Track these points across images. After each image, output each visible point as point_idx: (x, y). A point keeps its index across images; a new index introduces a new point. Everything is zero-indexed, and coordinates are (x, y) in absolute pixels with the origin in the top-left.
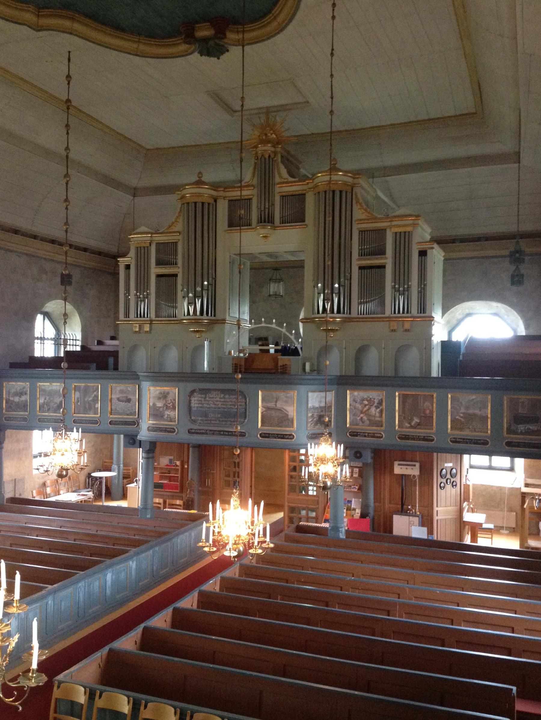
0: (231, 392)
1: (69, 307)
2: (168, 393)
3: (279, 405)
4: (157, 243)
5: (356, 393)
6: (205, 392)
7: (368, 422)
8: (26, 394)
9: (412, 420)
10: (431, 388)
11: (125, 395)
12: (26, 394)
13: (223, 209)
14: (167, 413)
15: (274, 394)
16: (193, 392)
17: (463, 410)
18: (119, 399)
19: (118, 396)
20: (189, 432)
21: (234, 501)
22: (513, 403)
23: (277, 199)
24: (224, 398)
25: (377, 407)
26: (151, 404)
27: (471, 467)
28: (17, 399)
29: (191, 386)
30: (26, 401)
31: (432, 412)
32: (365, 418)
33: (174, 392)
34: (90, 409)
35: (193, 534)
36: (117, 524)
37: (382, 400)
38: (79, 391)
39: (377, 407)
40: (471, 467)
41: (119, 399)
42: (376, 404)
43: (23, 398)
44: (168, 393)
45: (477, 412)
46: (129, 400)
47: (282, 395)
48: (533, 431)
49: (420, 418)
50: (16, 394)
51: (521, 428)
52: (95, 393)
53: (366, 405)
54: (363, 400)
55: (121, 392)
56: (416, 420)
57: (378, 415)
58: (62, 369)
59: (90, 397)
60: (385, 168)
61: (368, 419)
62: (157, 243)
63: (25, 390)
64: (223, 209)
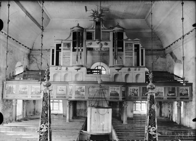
1: (195, 97)
2: (82, 87)
3: (115, 90)
5: (131, 87)
6: (93, 87)
7: (134, 95)
8: (27, 89)
9: (145, 94)
10: (137, 85)
11: (62, 89)
12: (27, 89)
15: (114, 87)
17: (157, 91)
18: (59, 90)
19: (59, 89)
23: (101, 32)
25: (136, 91)
26: (76, 90)
28: (23, 90)
32: (133, 94)
33: (84, 87)
39: (136, 91)
42: (136, 90)
43: (26, 90)
45: (161, 91)
46: (63, 90)
47: (116, 87)
48: (173, 95)
51: (170, 94)
52: (52, 88)
53: (133, 91)
57: (137, 93)
58: (98, 84)
61: (134, 94)
63: (27, 87)
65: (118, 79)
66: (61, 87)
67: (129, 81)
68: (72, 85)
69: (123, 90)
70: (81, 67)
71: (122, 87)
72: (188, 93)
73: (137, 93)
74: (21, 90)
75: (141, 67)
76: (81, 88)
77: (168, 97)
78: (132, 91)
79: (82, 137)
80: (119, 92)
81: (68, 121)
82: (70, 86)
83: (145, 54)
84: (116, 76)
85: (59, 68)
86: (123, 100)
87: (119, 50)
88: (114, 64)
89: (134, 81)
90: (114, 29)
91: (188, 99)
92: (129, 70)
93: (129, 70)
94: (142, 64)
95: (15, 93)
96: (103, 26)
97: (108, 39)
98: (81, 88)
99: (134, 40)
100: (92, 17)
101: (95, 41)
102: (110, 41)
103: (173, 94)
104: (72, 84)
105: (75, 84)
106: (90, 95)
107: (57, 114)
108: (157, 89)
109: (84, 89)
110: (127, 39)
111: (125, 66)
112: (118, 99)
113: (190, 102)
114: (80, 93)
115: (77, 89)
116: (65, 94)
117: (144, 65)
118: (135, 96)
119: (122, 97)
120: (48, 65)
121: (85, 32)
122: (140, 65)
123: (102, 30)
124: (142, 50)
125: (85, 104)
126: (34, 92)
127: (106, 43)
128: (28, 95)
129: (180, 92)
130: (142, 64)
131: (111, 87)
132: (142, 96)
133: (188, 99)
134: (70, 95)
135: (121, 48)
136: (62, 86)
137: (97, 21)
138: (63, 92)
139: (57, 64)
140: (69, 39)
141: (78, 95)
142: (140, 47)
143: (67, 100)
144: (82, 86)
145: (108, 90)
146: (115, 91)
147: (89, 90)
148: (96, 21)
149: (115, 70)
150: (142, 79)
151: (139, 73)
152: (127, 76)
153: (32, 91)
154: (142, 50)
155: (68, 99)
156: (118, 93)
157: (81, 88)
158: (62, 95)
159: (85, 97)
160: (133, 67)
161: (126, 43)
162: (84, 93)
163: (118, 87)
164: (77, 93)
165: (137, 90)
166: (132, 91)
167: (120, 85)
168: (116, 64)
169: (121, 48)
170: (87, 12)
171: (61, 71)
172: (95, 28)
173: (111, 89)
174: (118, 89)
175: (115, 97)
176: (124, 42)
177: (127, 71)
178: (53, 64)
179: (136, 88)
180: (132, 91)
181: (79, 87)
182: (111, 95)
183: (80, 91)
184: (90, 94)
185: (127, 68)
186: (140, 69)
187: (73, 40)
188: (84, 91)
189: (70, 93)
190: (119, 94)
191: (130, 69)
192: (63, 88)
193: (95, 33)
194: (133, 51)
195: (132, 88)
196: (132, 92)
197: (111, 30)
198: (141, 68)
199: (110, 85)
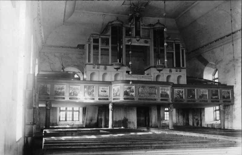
0: (151, 87)
3: (165, 91)
5: (176, 89)
7: (179, 97)
8: (64, 89)
9: (190, 96)
13: (124, 30)
14: (131, 93)
15: (164, 88)
17: (201, 93)
18: (102, 91)
20: (139, 99)
22: (212, 91)
25: (182, 93)
26: (125, 91)
27: (66, 120)
28: (60, 91)
30: (64, 91)
31: (195, 94)
38: (86, 88)
39: (182, 93)
40: (66, 120)
41: (102, 91)
43: (63, 90)
44: (131, 87)
45: (205, 94)
46: (105, 91)
47: (166, 88)
49: (192, 95)
50: (59, 89)
51: (214, 97)
54: (178, 91)
55: (103, 89)
56: (191, 96)
59: (91, 90)
60: (105, 29)
64: (124, 30)
65: (160, 80)
68: (120, 84)
69: (225, 95)
71: (124, 85)
72: (229, 95)
73: (183, 96)
74: (57, 90)
76: (130, 88)
77: (212, 100)
79: (150, 147)
80: (169, 92)
82: (114, 86)
84: (158, 76)
88: (155, 62)
89: (101, 80)
90: (154, 27)
91: (230, 102)
93: (171, 71)
94: (183, 66)
95: (49, 94)
96: (142, 23)
98: (130, 88)
102: (150, 39)
103: (216, 97)
105: (124, 84)
106: (140, 96)
108: (202, 91)
113: (231, 106)
115: (125, 89)
117: (185, 66)
118: (180, 98)
120: (62, 65)
122: (181, 66)
123: (141, 27)
124: (183, 51)
125: (158, 110)
126: (72, 93)
127: (145, 40)
128: (65, 96)
129: (223, 94)
132: (188, 98)
133: (230, 102)
142: (180, 47)
144: (130, 86)
148: (136, 16)
150: (183, 81)
151: (94, 72)
152: (168, 77)
153: (71, 91)
154: (183, 51)
155: (111, 101)
157: (130, 88)
159: (135, 98)
162: (134, 94)
164: (126, 93)
165: (182, 92)
166: (177, 93)
167: (170, 86)
168: (158, 64)
177: (168, 72)
179: (181, 90)
182: (161, 97)
183: (129, 91)
187: (111, 36)
188: (133, 92)
195: (177, 89)
196: (178, 95)
197: (152, 27)
198: (182, 69)
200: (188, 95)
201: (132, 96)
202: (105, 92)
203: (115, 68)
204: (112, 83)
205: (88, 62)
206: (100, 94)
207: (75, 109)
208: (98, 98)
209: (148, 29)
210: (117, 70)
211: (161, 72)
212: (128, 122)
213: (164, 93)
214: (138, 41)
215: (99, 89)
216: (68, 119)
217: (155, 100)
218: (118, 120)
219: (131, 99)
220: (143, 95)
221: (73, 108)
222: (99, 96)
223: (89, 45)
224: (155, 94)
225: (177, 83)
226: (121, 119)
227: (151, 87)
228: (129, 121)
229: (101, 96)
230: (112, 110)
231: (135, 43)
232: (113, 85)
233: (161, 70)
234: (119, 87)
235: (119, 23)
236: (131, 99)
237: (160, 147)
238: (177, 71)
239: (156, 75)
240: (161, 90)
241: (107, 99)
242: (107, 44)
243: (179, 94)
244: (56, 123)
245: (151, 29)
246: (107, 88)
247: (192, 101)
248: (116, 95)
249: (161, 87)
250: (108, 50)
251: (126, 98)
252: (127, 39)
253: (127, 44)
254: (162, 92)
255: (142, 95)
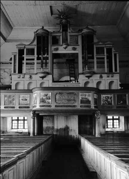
0: (70, 93)
2: (47, 94)
3: (86, 97)
4: (26, 49)
7: (107, 104)
9: (121, 102)
15: (85, 94)
16: (57, 94)
18: (22, 100)
21: (75, 138)
24: (68, 95)
26: (41, 98)
29: (55, 92)
32: (107, 102)
33: (50, 94)
34: (11, 103)
35: (42, 146)
36: (18, 109)
37: (112, 97)
39: (110, 99)
44: (47, 94)
46: (26, 100)
47: (87, 94)
55: (23, 97)
56: (122, 102)
57: (111, 101)
62: (26, 49)
65: (89, 85)
66: (24, 96)
67: (102, 87)
68: (36, 92)
70: (46, 74)
71: (95, 93)
73: (112, 101)
75: (114, 73)
77: (56, 104)
78: (105, 99)
80: (90, 99)
81: (32, 135)
83: (119, 66)
84: (87, 83)
85: (22, 76)
86: (96, 109)
87: (89, 58)
88: (83, 70)
89: (107, 88)
92: (101, 77)
93: (101, 77)
94: (116, 70)
97: (77, 43)
98: (46, 95)
99: (106, 43)
100: (58, 19)
101: (62, 45)
102: (79, 45)
104: (36, 91)
105: (40, 91)
106: (57, 103)
107: (22, 132)
109: (50, 96)
110: (98, 42)
111: (97, 72)
112: (90, 107)
114: (45, 100)
115: (42, 96)
116: (28, 104)
117: (118, 71)
119: (94, 104)
121: (51, 36)
124: (115, 55)
127: (74, 47)
130: (116, 70)
131: (82, 93)
132: (117, 104)
134: (34, 104)
135: (91, 55)
136: (26, 94)
137: (64, 23)
138: (26, 101)
139: (20, 71)
140: (34, 44)
141: (43, 103)
142: (113, 51)
143: (31, 111)
145: (78, 96)
146: (86, 98)
147: (55, 97)
149: (85, 77)
150: (116, 86)
151: (19, 81)
152: (99, 83)
154: (115, 55)
156: (90, 100)
158: (26, 105)
160: (106, 73)
161: (96, 48)
163: (90, 94)
164: (42, 101)
165: (111, 97)
167: (92, 92)
169: (91, 55)
170: (53, 15)
171: (24, 80)
172: (61, 31)
173: (81, 95)
174: (89, 96)
175: (86, 105)
176: (95, 46)
177: (99, 79)
178: (15, 72)
179: (109, 96)
180: (105, 99)
181: (45, 94)
182: (81, 103)
184: (57, 102)
185: (99, 75)
186: (113, 75)
188: (50, 99)
189: (35, 102)
190: (90, 101)
191: (102, 75)
192: (26, 97)
193: (61, 37)
194: (105, 56)
195: (105, 95)
196: (106, 101)
197: (80, 33)
198: (114, 75)
199: (80, 91)
200: (119, 101)
201: (49, 103)
202: (25, 101)
203: (41, 77)
204: (33, 91)
205: (13, 72)
206: (20, 102)
207: (20, 118)
208: (4, 106)
209: (77, 36)
210: (89, 79)
211: (91, 78)
212: (69, 130)
213: (84, 99)
214: (65, 48)
215: (19, 98)
216: (19, 127)
217: (74, 106)
218: (59, 128)
219: (47, 106)
220: (61, 102)
221: (113, 117)
222: (19, 104)
223: (14, 56)
224: (75, 100)
225: (108, 89)
226: (62, 127)
227: (70, 93)
228: (70, 128)
229: (22, 105)
230: (33, 118)
231: (62, 50)
232: (34, 93)
233: (91, 76)
234: (36, 94)
235: (88, 30)
236: (47, 106)
237: (13, 154)
238: (108, 77)
239: (85, 82)
240: (81, 96)
241: (28, 107)
242: (33, 54)
243: (107, 101)
244: (7, 131)
245: (79, 35)
246: (27, 96)
247: (123, 107)
248: (34, 104)
249: (81, 92)
250: (104, 58)
251: (42, 105)
252: (53, 47)
253: (54, 52)
254: (82, 98)
255: (59, 102)
